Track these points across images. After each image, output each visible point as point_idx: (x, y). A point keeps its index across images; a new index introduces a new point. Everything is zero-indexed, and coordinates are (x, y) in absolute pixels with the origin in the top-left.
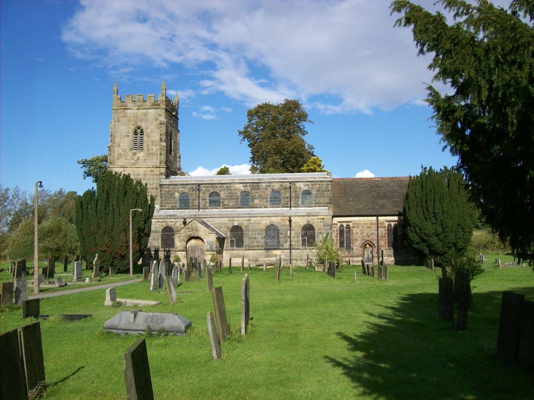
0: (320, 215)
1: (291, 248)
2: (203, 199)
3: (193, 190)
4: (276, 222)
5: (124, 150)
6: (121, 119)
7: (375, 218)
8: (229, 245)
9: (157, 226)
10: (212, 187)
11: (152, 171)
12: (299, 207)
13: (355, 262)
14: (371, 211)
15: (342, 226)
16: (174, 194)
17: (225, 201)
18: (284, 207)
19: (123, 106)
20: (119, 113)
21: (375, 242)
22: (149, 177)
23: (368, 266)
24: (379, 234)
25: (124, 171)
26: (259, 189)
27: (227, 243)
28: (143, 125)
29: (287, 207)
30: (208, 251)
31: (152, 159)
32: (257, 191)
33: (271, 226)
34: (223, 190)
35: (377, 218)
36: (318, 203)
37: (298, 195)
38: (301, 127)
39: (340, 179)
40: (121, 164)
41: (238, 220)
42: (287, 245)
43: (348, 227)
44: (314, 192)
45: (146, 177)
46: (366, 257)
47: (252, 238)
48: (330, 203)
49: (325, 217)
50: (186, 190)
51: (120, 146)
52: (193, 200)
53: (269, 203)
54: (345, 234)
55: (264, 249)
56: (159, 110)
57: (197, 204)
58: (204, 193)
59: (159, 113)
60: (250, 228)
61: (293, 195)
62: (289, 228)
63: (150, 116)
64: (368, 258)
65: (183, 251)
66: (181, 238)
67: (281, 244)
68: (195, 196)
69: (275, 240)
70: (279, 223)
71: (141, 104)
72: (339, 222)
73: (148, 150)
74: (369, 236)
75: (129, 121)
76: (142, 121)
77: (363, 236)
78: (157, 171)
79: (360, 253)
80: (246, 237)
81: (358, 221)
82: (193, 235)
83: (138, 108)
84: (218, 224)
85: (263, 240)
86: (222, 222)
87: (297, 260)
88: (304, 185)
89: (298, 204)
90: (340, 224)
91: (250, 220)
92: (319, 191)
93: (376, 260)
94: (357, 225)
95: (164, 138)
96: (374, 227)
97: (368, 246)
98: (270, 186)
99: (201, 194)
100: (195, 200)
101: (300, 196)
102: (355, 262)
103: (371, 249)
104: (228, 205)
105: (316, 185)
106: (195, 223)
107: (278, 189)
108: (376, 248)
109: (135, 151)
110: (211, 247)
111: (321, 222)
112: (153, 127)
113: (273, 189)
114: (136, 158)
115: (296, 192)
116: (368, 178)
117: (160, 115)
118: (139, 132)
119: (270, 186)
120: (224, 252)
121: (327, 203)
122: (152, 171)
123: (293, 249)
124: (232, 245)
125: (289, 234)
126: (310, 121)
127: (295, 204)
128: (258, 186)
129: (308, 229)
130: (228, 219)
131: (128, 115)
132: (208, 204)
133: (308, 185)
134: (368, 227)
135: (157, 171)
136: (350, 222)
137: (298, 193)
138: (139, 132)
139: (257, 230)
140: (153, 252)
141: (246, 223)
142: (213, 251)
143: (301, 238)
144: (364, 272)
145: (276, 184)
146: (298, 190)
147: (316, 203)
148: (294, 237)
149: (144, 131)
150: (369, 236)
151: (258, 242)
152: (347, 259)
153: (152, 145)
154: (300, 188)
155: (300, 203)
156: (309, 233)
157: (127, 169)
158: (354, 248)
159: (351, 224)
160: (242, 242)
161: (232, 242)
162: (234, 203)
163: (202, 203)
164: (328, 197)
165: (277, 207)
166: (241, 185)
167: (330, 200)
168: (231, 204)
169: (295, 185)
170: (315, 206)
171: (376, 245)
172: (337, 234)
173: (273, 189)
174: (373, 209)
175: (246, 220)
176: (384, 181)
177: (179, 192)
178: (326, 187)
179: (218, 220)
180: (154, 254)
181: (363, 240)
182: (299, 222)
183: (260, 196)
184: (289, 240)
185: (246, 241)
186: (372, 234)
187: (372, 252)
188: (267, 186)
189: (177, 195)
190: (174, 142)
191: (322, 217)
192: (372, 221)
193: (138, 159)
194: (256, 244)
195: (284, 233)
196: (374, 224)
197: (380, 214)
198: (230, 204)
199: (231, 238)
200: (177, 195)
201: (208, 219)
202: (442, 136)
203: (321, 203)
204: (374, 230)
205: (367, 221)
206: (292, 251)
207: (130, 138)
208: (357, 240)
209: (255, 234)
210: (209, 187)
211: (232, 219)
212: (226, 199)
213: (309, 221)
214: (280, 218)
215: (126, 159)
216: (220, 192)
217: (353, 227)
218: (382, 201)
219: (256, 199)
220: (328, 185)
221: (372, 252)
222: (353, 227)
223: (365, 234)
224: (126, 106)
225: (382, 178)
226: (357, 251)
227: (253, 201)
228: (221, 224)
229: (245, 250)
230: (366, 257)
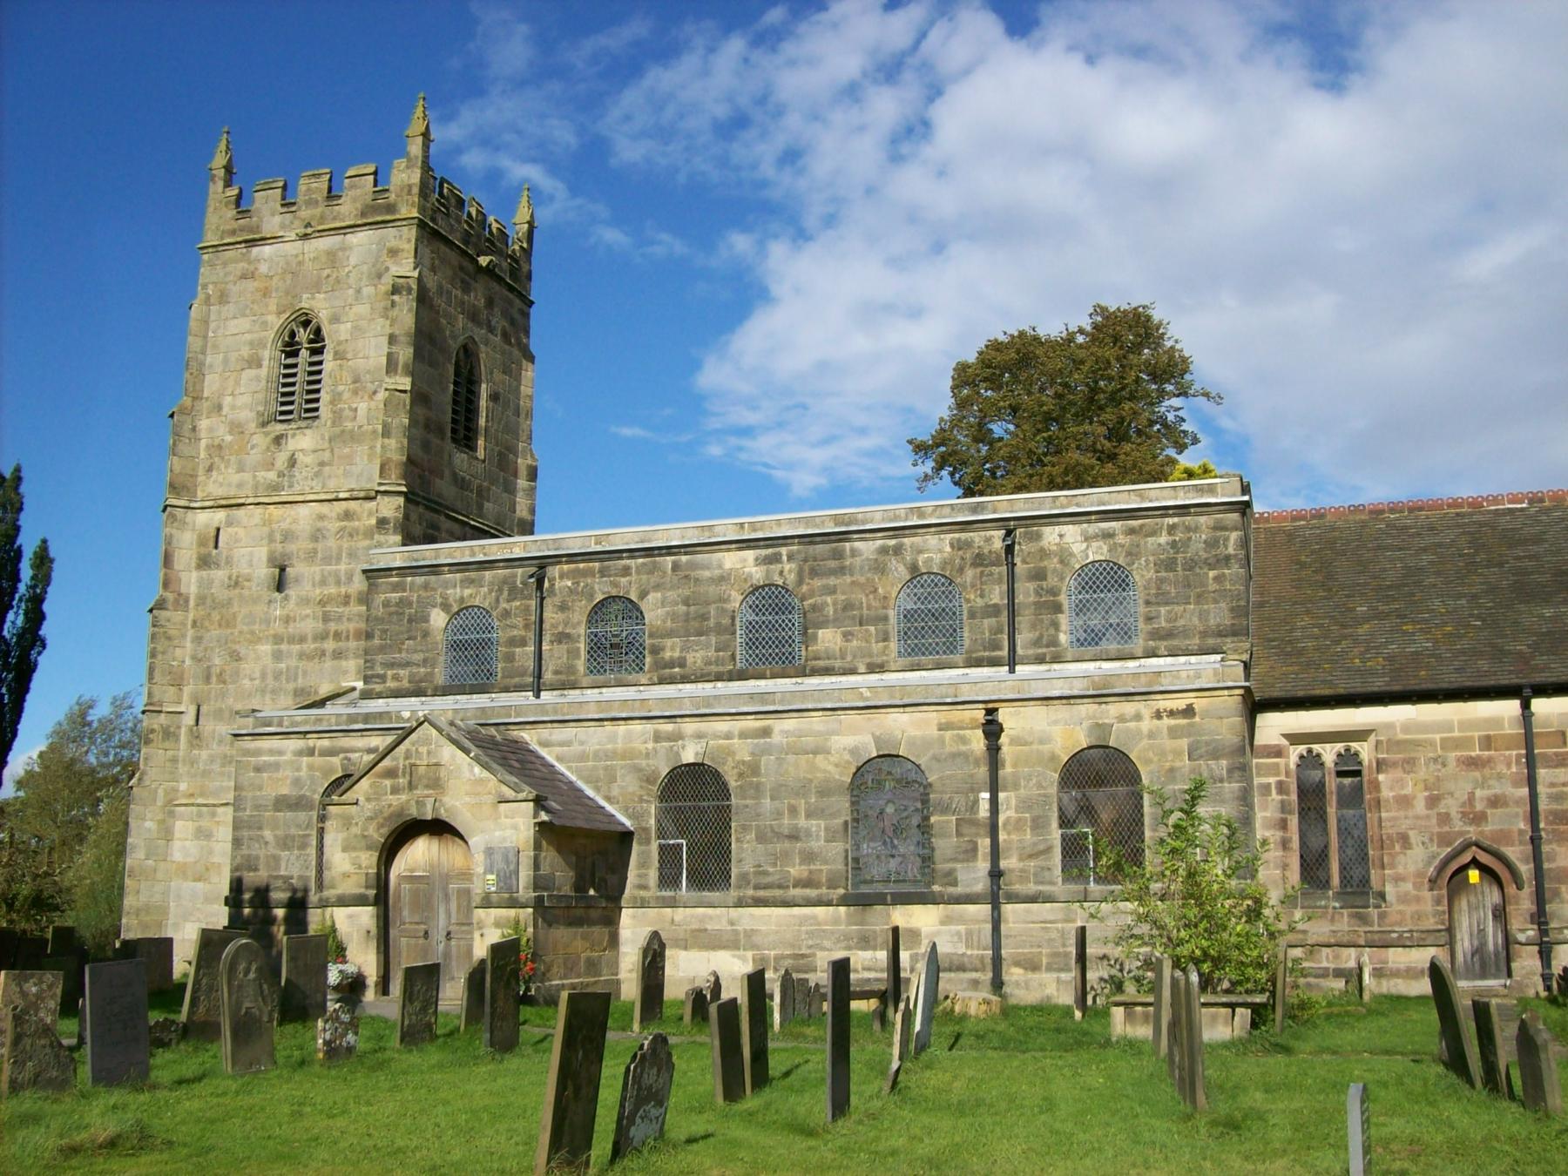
0: (1172, 701)
1: (996, 893)
2: (562, 637)
3: (514, 593)
4: (912, 743)
5: (236, 428)
6: (234, 289)
7: (1512, 707)
8: (653, 875)
9: (303, 773)
11: (347, 515)
12: (1057, 659)
13: (1396, 974)
14: (1484, 665)
15: (1311, 761)
16: (426, 619)
17: (669, 642)
18: (978, 663)
19: (242, 230)
20: (225, 264)
21: (1516, 853)
22: (332, 543)
23: (1481, 1011)
24: (1543, 805)
25: (229, 524)
26: (841, 571)
27: (642, 868)
28: (321, 307)
29: (994, 663)
30: (487, 903)
31: (349, 460)
32: (832, 581)
33: (885, 765)
34: (657, 587)
35: (1526, 706)
36: (1169, 635)
37: (1054, 592)
38: (1171, 417)
39: (1297, 516)
40: (220, 492)
41: (699, 736)
42: (975, 876)
43: (1349, 768)
44: (1142, 574)
45: (320, 546)
46: (1464, 944)
47: (779, 836)
48: (1235, 632)
49: (1200, 703)
50: (480, 595)
51: (219, 407)
52: (513, 642)
53: (893, 645)
54: (1332, 810)
55: (845, 901)
56: (390, 232)
57: (530, 664)
58: (563, 608)
59: (393, 243)
60: (767, 780)
61: (1026, 592)
62: (983, 771)
63: (353, 261)
64: (1479, 951)
65: (360, 901)
66: (355, 830)
67: (942, 866)
68: (519, 621)
69: (907, 848)
70: (927, 743)
71: (318, 211)
72: (1295, 739)
73: (338, 417)
74: (1479, 818)
75: (266, 293)
76: (316, 287)
77: (1445, 818)
78: (367, 514)
79: (1431, 923)
80: (745, 828)
81: (1406, 728)
82: (414, 812)
83: (302, 231)
84: (597, 756)
85: (838, 847)
86: (620, 745)
87: (1032, 966)
88: (1087, 539)
89: (1054, 642)
90: (1302, 749)
91: (766, 732)
92: (1170, 565)
93: (1527, 963)
94: (1401, 752)
95: (405, 353)
96: (1510, 762)
97: (1474, 875)
98: (897, 550)
99: (550, 614)
100: (523, 643)
101: (1063, 598)
102: (1396, 974)
103: (1492, 896)
104: (682, 663)
105: (1153, 533)
106: (427, 741)
107: (945, 563)
108: (1528, 890)
109: (280, 428)
110: (507, 880)
111: (1173, 733)
112: (362, 309)
113: (914, 569)
114: (281, 459)
115: (1039, 575)
116: (1455, 504)
117: (394, 252)
118: (303, 341)
119: (897, 550)
120: (626, 916)
121: (1220, 634)
122: (347, 515)
123: (1015, 898)
124: (668, 879)
125: (984, 810)
126: (1207, 395)
127: (1037, 643)
128: (838, 555)
129: (1098, 773)
130: (650, 727)
131: (263, 268)
132: (581, 665)
133: (1108, 535)
134: (1472, 763)
135: (367, 514)
136: (1361, 735)
137: (1052, 581)
138: (303, 341)
139: (802, 789)
140: (280, 913)
141: (743, 750)
142: (513, 903)
143: (1056, 834)
144: (1456, 1062)
145: (932, 540)
146: (1053, 564)
147: (1156, 635)
148: (1018, 825)
149: (325, 332)
150: (1479, 818)
151: (809, 857)
152: (1349, 958)
153: (355, 392)
154: (1064, 556)
155: (1063, 638)
156: (1107, 805)
157: (241, 512)
158: (1389, 889)
159: (1365, 750)
160: (724, 855)
161: (669, 856)
162: (712, 653)
163: (554, 656)
164: (1222, 593)
165: (939, 666)
166: (750, 555)
167: (1239, 612)
168: (696, 658)
169: (1039, 536)
170: (1152, 654)
171: (1525, 869)
172: (1284, 807)
173: (914, 569)
174: (1499, 654)
175: (743, 735)
176: (1547, 511)
177: (445, 607)
178: (1211, 544)
179: (594, 738)
180: (287, 919)
181: (1444, 840)
182: (1046, 733)
183: (848, 606)
184: (984, 843)
185: (745, 853)
186: (1495, 802)
187: (1500, 914)
188: (884, 551)
189: (438, 619)
190: (494, 397)
191: (1179, 703)
192: (1496, 722)
193: (292, 462)
194: (796, 870)
195: (959, 801)
196: (1509, 743)
197: (1540, 678)
198: (690, 658)
199: (661, 834)
200: (438, 619)
201: (544, 732)
203: (1185, 633)
204: (1506, 779)
205: (1463, 725)
206: (1008, 909)
207: (264, 372)
208: (1405, 840)
209: (793, 811)
210: (591, 573)
211: (668, 727)
212: (670, 634)
213: (1104, 729)
214: (933, 717)
215: (241, 470)
216: (643, 595)
217: (1380, 765)
218: (1548, 612)
219: (823, 624)
220: (1219, 527)
221: (1500, 914)
222: (1380, 765)
223: (1452, 806)
224: (258, 229)
225: (1535, 499)
226: (1409, 909)
227: (807, 638)
228: (613, 755)
229: (740, 904)
230: (1464, 944)
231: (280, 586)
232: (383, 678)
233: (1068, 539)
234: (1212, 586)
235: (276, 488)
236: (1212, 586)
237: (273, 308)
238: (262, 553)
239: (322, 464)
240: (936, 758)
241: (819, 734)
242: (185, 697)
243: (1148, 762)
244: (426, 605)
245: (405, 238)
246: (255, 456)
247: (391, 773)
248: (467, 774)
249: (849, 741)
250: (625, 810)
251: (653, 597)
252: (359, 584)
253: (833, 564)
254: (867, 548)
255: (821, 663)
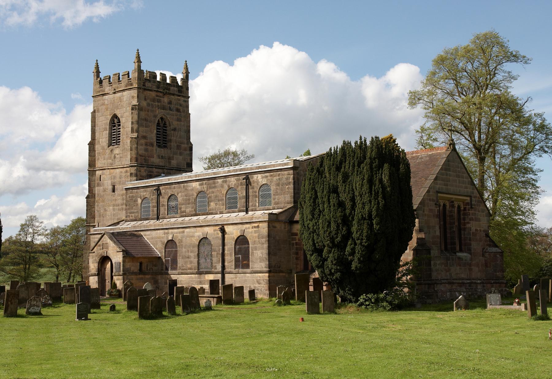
6: (100, 108)
10: (170, 188)
17: (183, 206)
26: (215, 187)
32: (213, 190)
34: (181, 192)
44: (273, 187)
67: (214, 265)
69: (208, 260)
76: (117, 108)
80: (180, 256)
83: (113, 91)
98: (226, 182)
111: (255, 232)
114: (113, 156)
131: (106, 102)
133: (267, 177)
154: (258, 182)
157: (105, 171)
166: (198, 183)
168: (188, 210)
175: (180, 233)
177: (141, 198)
183: (216, 196)
191: (256, 225)
194: (189, 266)
202: (442, 54)
209: (188, 251)
211: (166, 231)
212: (182, 205)
215: (104, 159)
216: (178, 194)
224: (104, 91)
231: (114, 191)
232: (129, 216)
233: (259, 178)
234: (287, 190)
235: (112, 164)
236: (287, 190)
237: (109, 114)
238: (110, 182)
239: (121, 157)
240: (213, 238)
241: (193, 232)
242: (96, 221)
243: (250, 239)
244: (137, 197)
245: (134, 93)
246: (107, 156)
247: (100, 246)
248: (112, 245)
249: (197, 234)
250: (159, 251)
251: (180, 194)
252: (125, 192)
253: (213, 185)
254: (220, 181)
255: (211, 211)
